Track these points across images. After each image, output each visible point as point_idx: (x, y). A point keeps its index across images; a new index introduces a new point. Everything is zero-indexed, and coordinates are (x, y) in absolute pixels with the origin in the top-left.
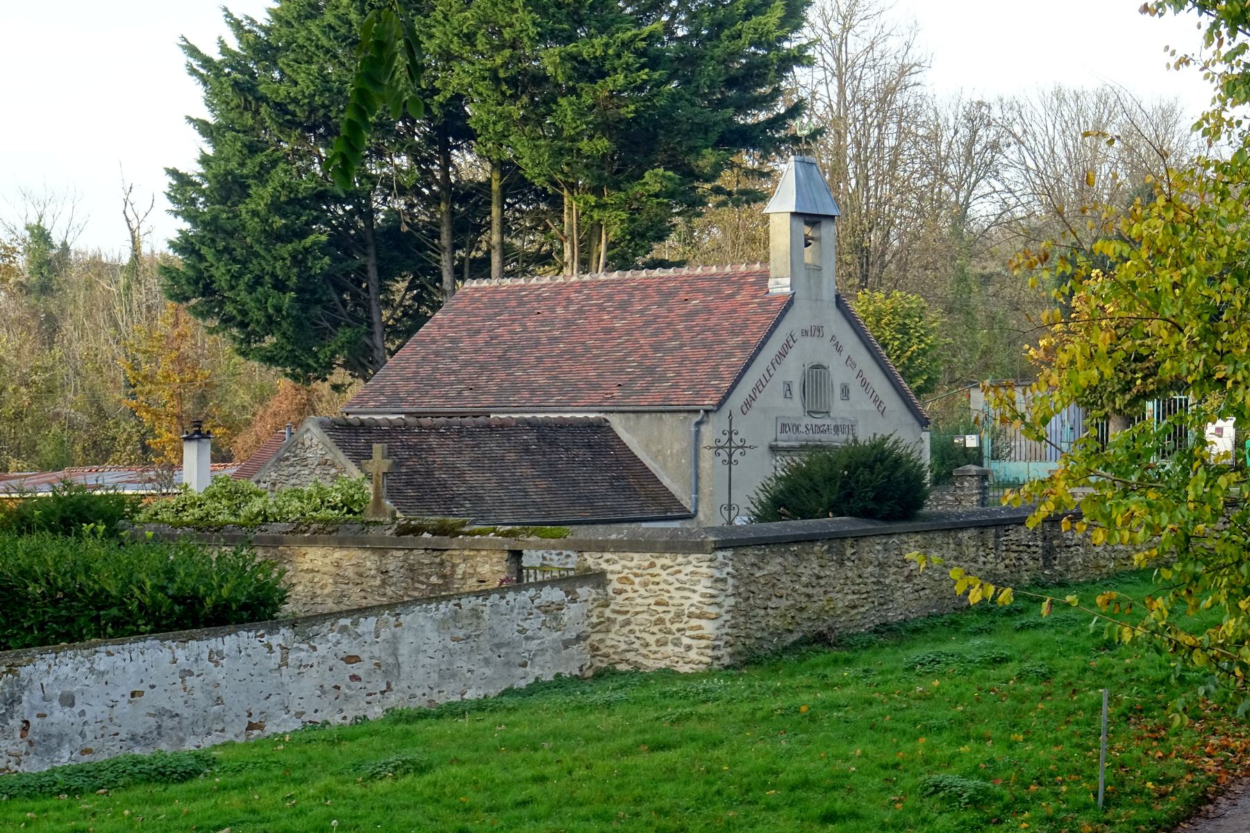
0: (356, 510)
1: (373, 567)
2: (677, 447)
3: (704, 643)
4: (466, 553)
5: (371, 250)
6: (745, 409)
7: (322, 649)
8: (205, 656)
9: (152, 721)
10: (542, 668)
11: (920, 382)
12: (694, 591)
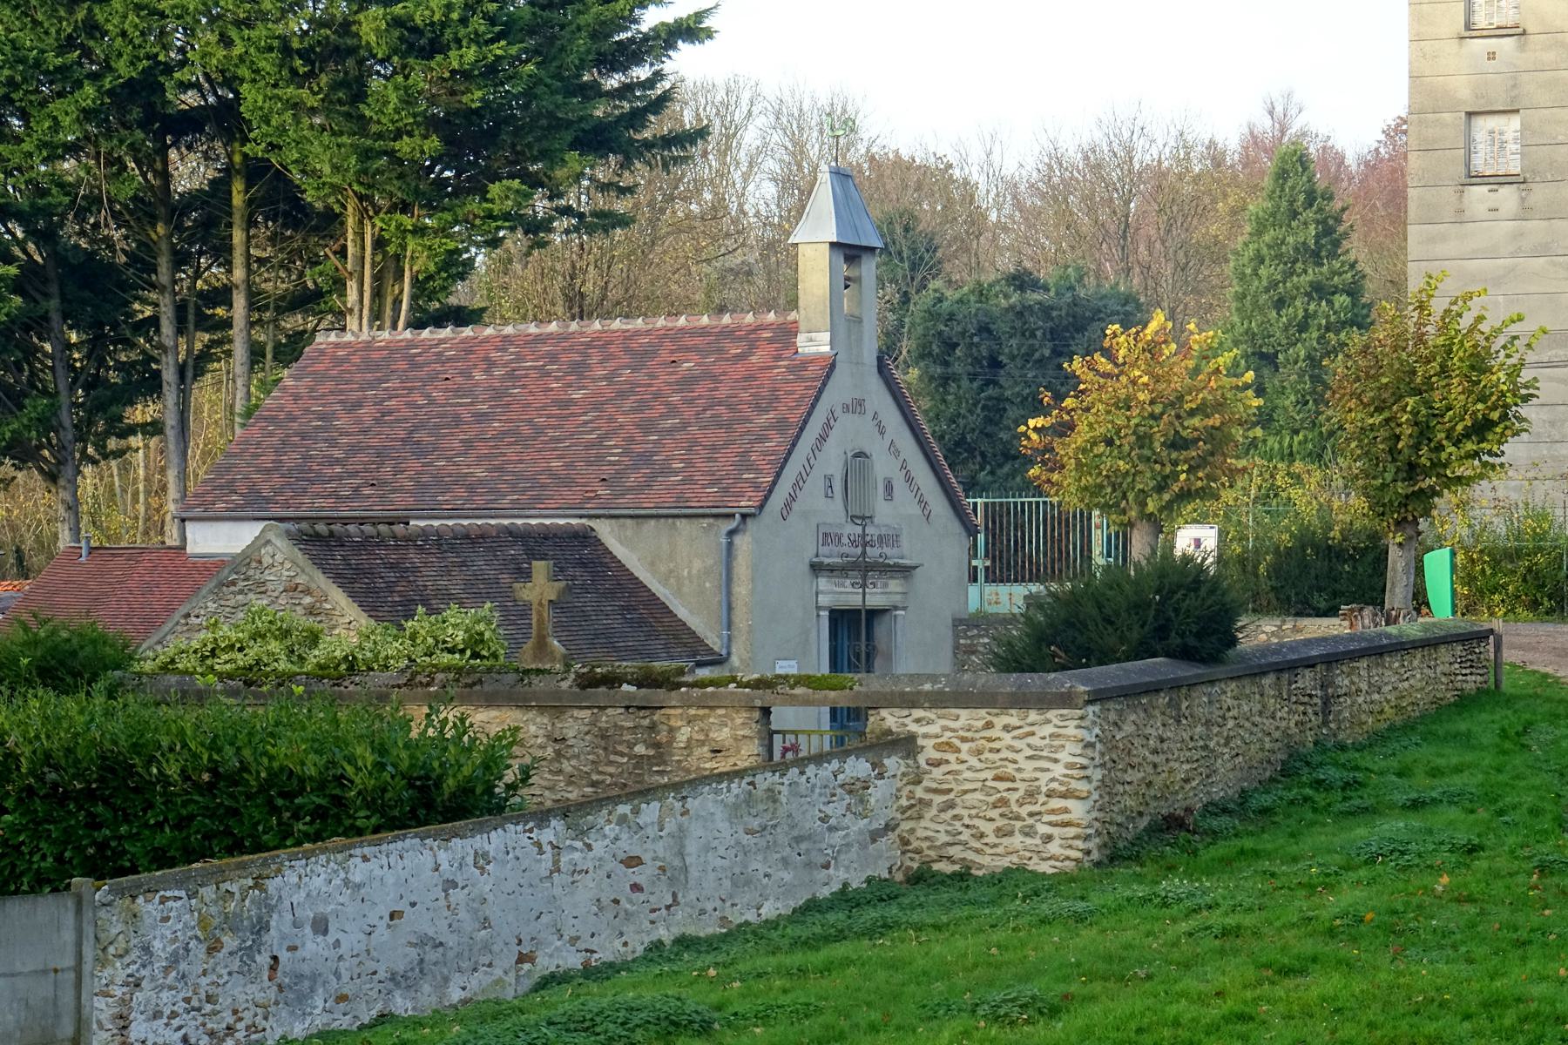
0: (484, 653)
1: (541, 732)
2: (697, 565)
3: (1072, 831)
4: (692, 712)
5: (54, 289)
7: (599, 847)
8: (470, 860)
9: (413, 953)
10: (847, 868)
12: (1056, 761)
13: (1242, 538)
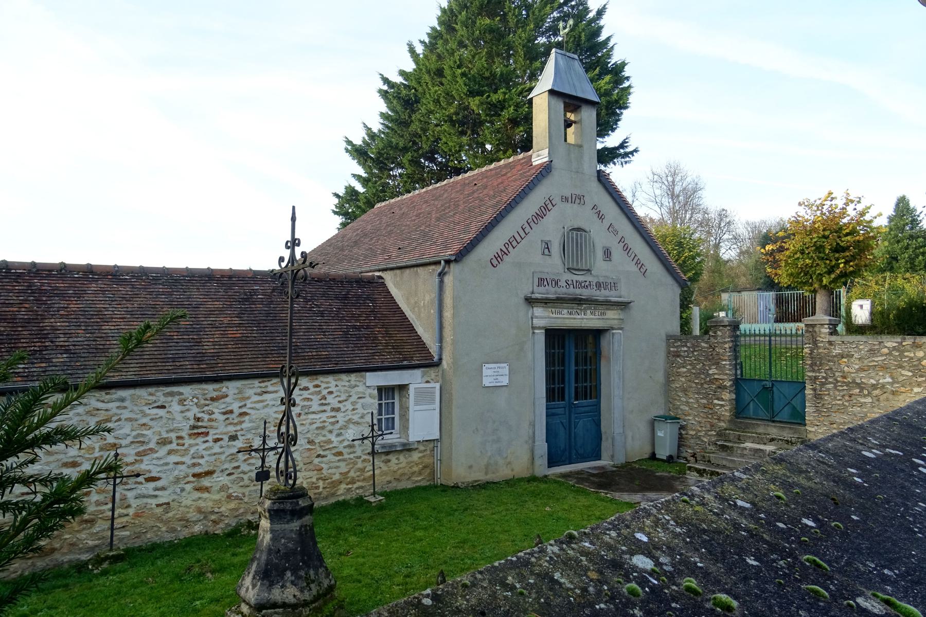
2: (427, 298)
6: (495, 262)
11: (690, 274)
13: (882, 304)
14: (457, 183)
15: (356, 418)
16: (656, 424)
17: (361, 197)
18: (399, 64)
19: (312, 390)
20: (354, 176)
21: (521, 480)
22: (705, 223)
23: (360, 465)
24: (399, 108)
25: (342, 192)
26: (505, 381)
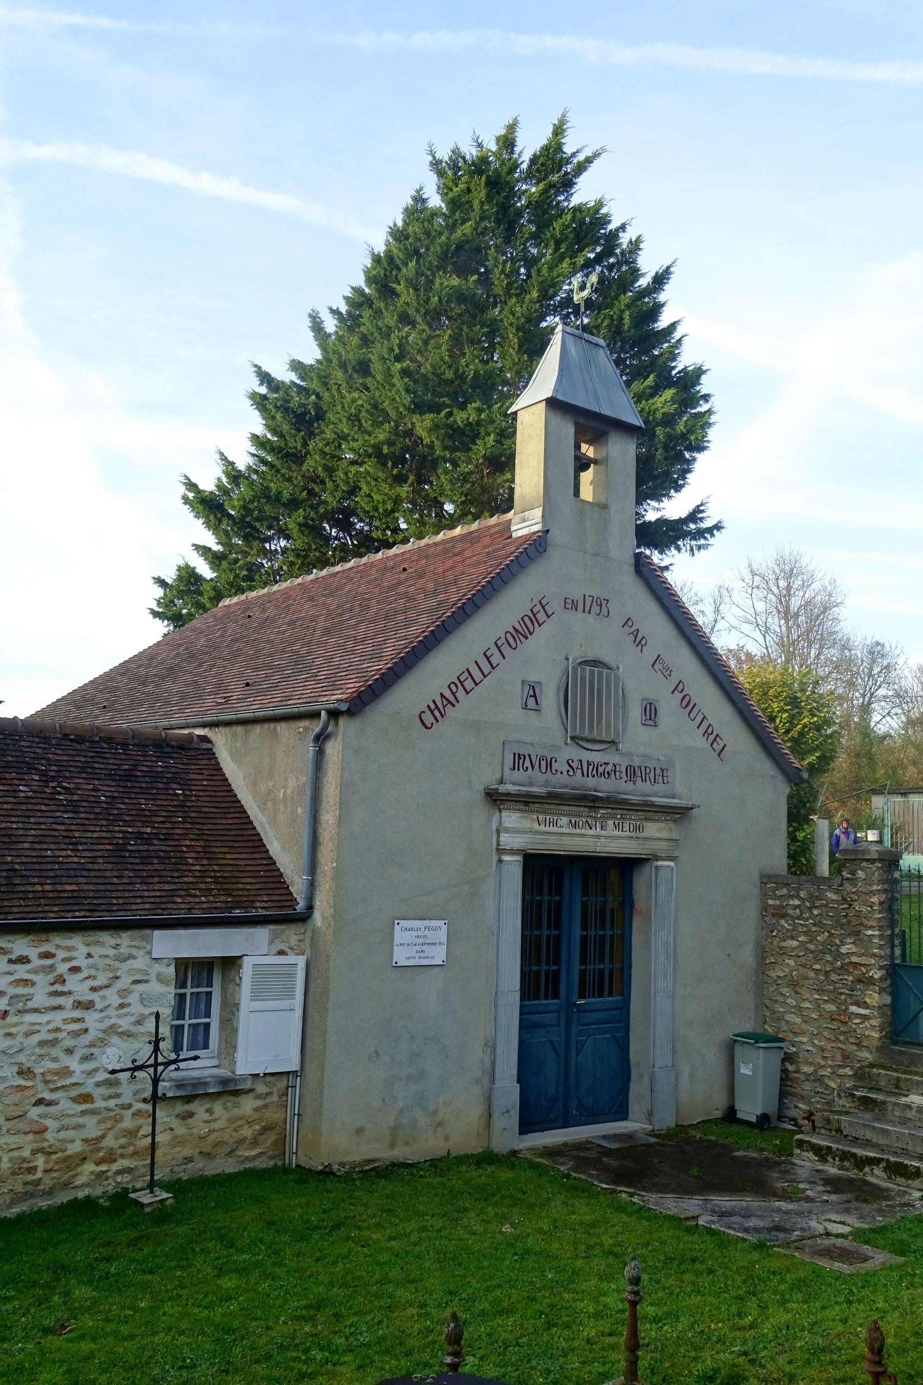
2: (292, 783)
6: (428, 718)
11: (812, 758)
14: (372, 565)
15: (125, 1024)
16: (738, 1049)
17: (206, 587)
18: (291, 350)
19: (36, 962)
20: (197, 547)
21: (462, 1160)
22: (844, 665)
23: (128, 1123)
24: (286, 427)
25: (170, 576)
26: (439, 955)
